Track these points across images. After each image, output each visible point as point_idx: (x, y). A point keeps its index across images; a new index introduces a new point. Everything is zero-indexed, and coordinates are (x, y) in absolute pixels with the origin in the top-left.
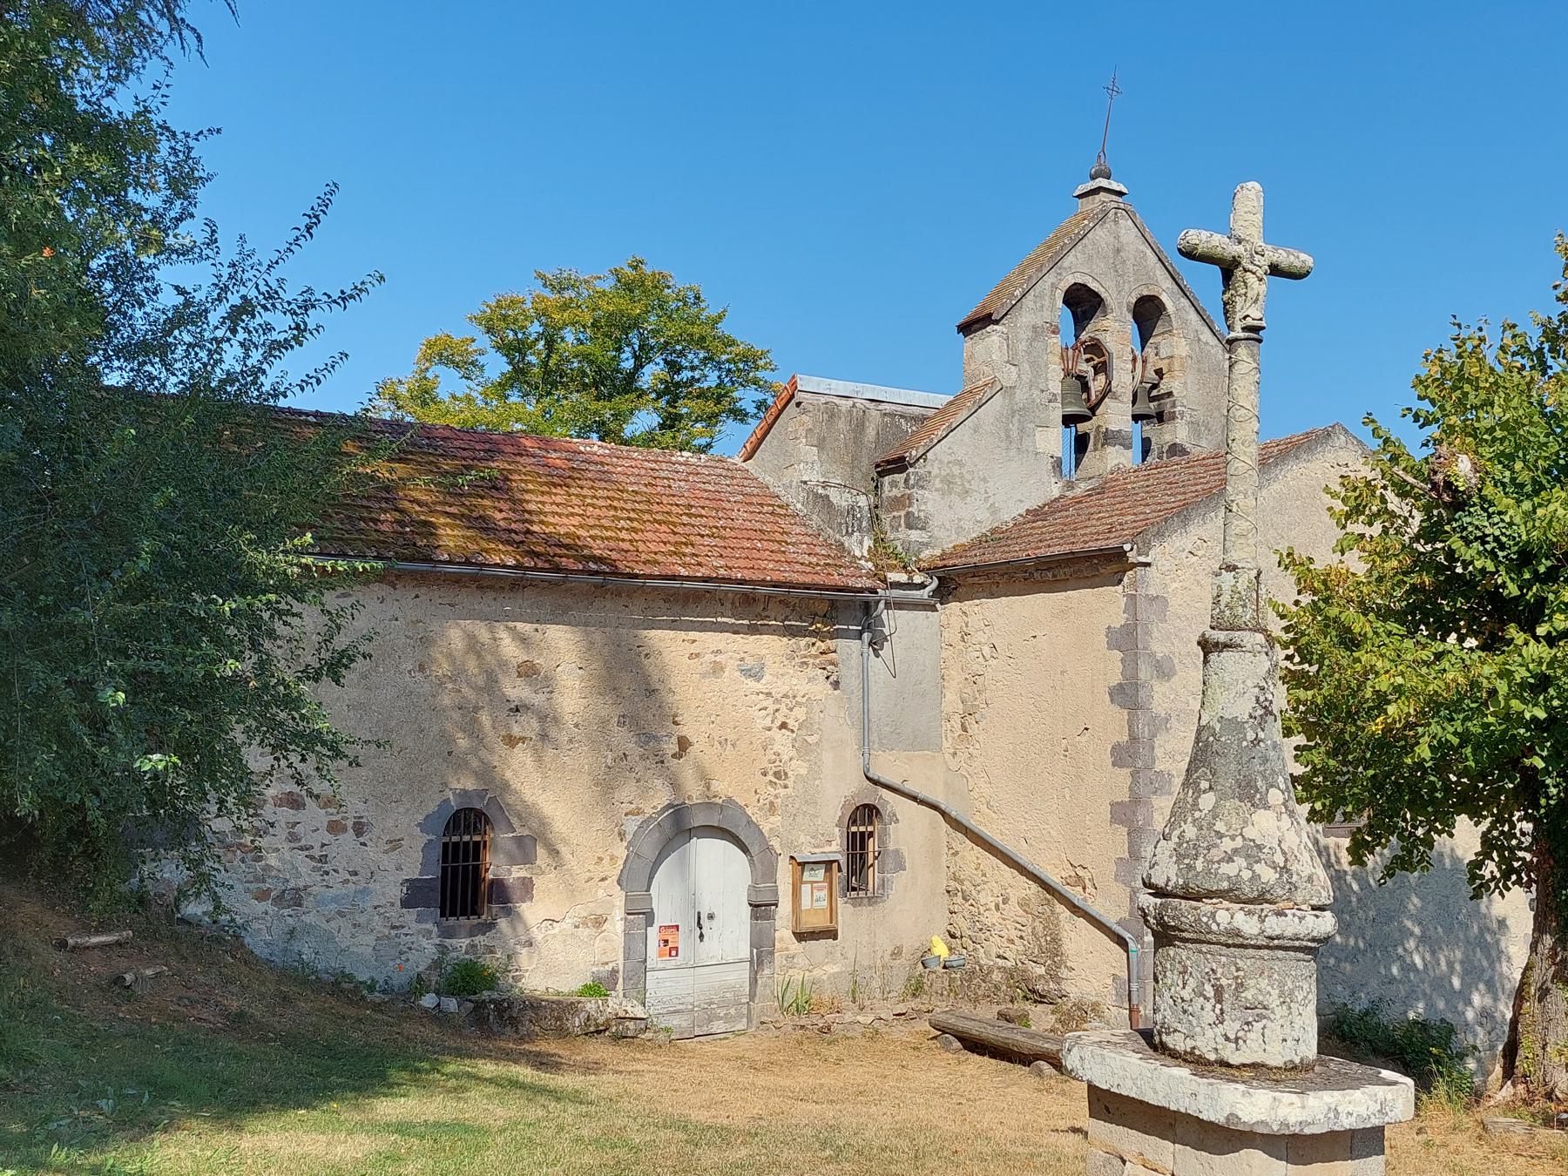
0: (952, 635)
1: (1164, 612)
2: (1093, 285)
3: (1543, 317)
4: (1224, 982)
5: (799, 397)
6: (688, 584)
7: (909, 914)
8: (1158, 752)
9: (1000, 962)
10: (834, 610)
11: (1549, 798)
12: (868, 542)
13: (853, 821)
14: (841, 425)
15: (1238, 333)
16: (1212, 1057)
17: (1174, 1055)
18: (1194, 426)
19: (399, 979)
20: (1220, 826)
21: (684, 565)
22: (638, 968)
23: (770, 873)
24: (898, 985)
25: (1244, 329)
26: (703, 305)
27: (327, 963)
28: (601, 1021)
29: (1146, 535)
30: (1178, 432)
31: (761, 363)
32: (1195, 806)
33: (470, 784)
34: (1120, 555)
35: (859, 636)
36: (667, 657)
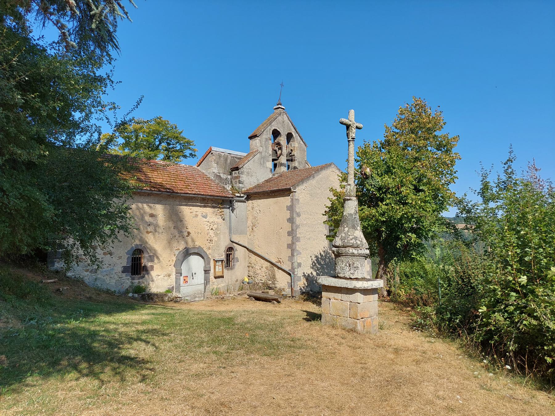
2: (278, 130)
5: (212, 152)
6: (191, 195)
7: (239, 272)
8: (297, 233)
10: (223, 202)
12: (230, 187)
14: (222, 159)
15: (350, 139)
17: (341, 278)
20: (349, 234)
24: (237, 288)
27: (105, 287)
32: (344, 230)
33: (137, 242)
34: (290, 189)
36: (185, 213)
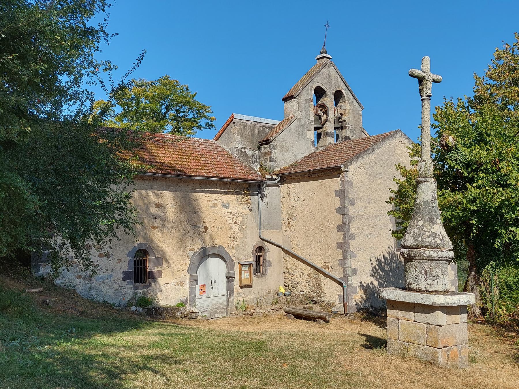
0: (285, 194)
1: (352, 185)
2: (323, 87)
3: (467, 97)
4: (427, 270)
5: (234, 120)
6: (208, 179)
7: (273, 281)
8: (351, 227)
9: (302, 293)
10: (250, 187)
11: (473, 233)
12: (259, 166)
13: (256, 252)
14: (247, 129)
15: (424, 97)
16: (424, 289)
17: (413, 290)
18: (352, 130)
19: (123, 303)
20: (425, 229)
21: (206, 173)
22: (193, 299)
23: (233, 268)
24: (270, 302)
25: (426, 96)
26: (189, 91)
27: (101, 298)
28: (185, 313)
29: (346, 163)
30: (347, 133)
31: (207, 110)
32: (417, 224)
33: (141, 241)
34: (339, 168)
35: (257, 195)
36: (201, 202)
